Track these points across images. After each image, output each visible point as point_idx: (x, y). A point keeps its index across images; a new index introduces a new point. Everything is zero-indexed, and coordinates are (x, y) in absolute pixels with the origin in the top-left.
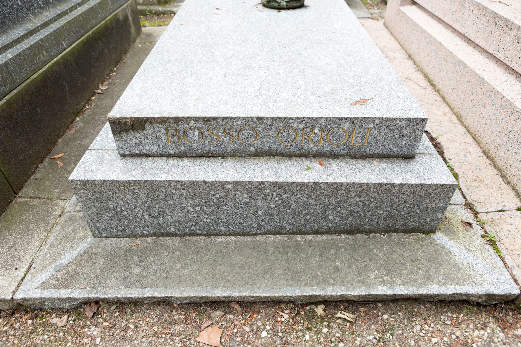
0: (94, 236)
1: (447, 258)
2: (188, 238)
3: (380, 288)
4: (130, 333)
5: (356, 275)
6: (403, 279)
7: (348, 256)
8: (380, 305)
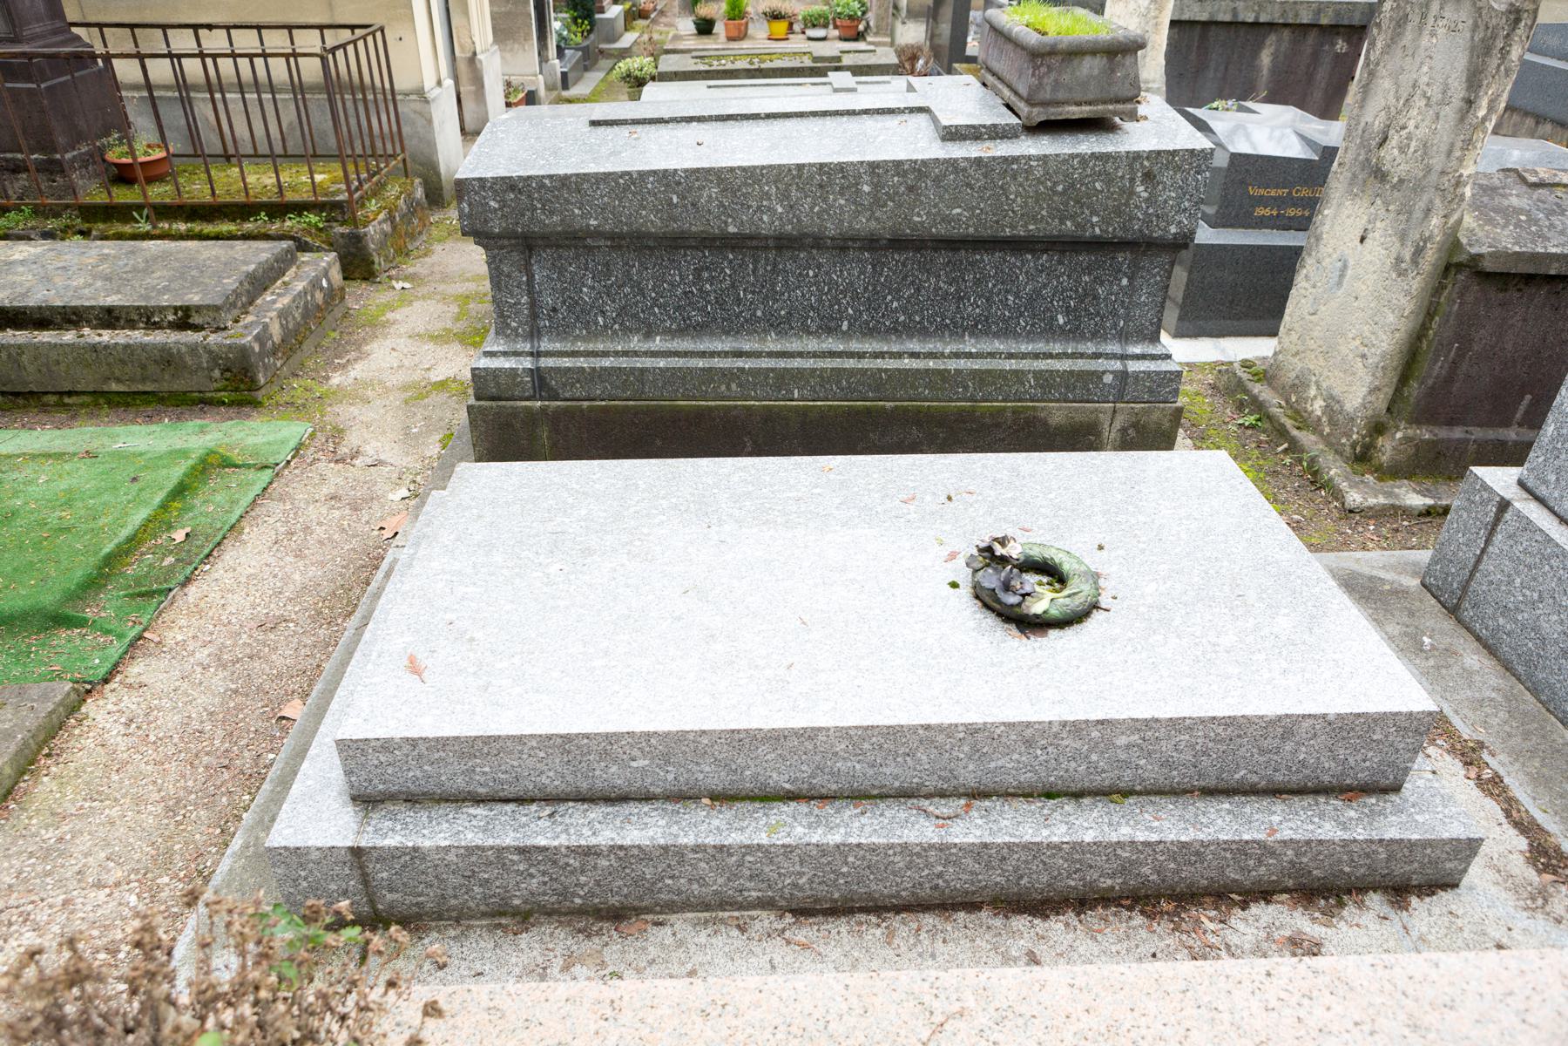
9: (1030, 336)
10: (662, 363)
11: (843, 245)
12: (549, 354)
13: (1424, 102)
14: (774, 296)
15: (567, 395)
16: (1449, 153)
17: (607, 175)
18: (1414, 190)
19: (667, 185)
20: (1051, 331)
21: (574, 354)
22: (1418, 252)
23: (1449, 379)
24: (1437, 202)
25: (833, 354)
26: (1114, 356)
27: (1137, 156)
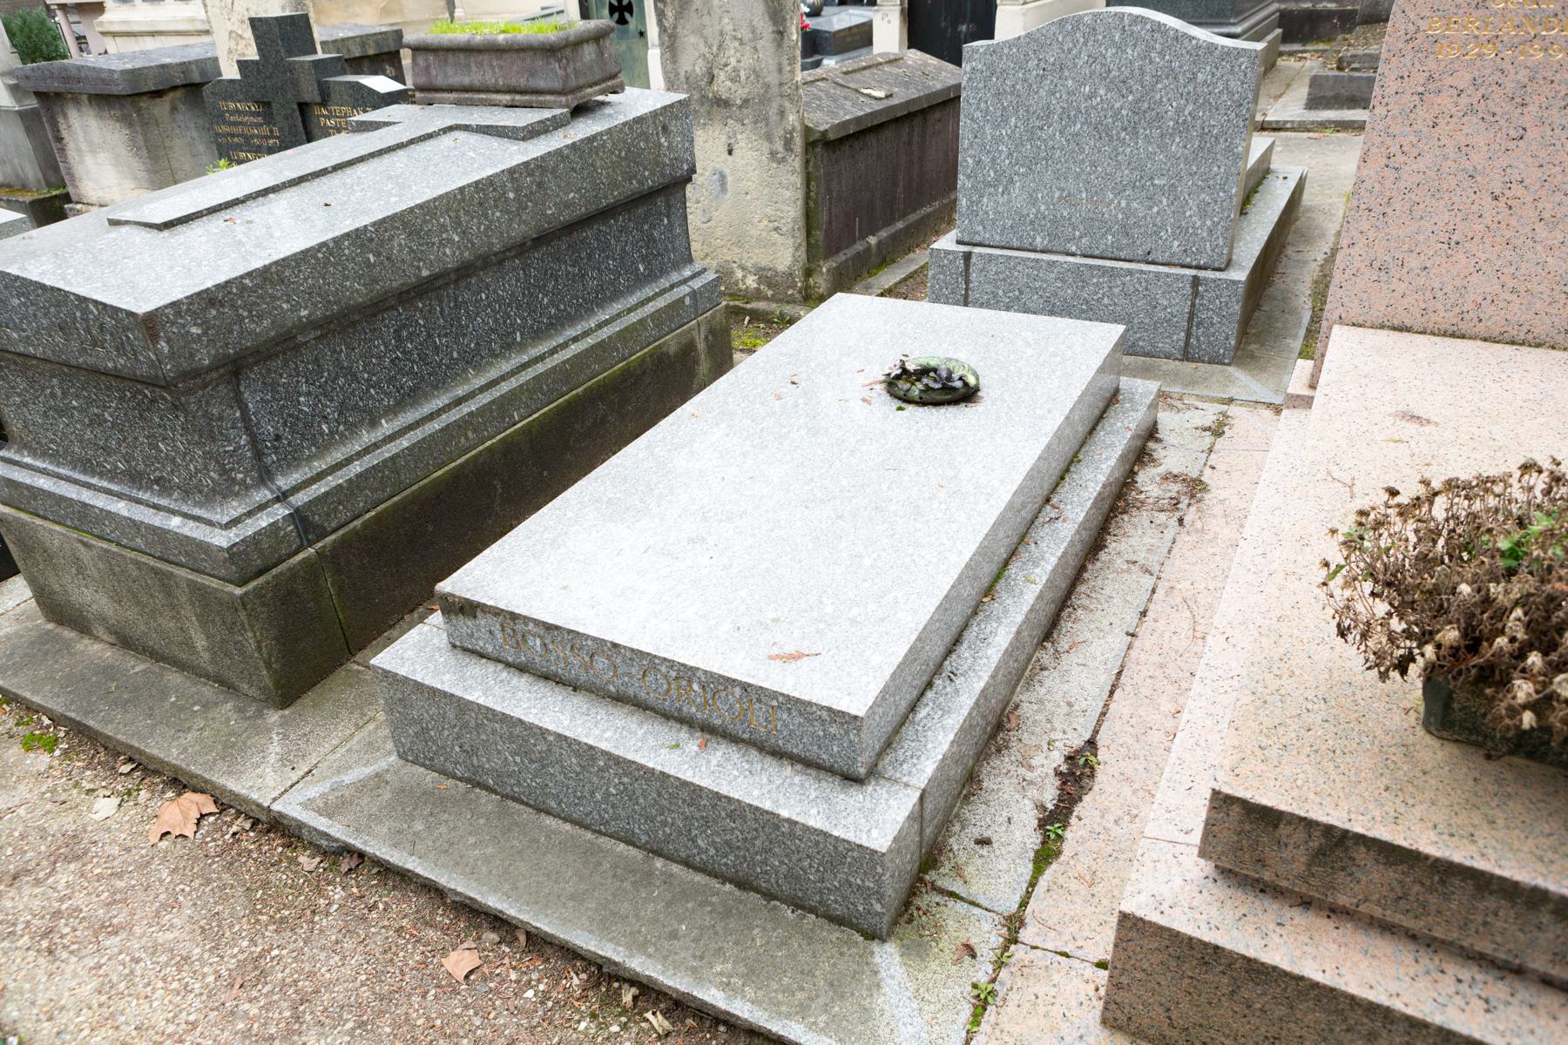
0: (400, 756)
1: (865, 993)
2: (510, 803)
3: (713, 991)
4: (374, 915)
5: (694, 957)
6: (760, 993)
7: (708, 921)
8: (722, 1028)
9: (630, 290)
10: (405, 443)
12: (296, 489)
13: (736, 44)
15: (334, 525)
16: (780, 70)
17: (305, 252)
18: (761, 103)
19: (362, 245)
21: (320, 476)
22: (788, 144)
24: (787, 104)
25: (525, 366)
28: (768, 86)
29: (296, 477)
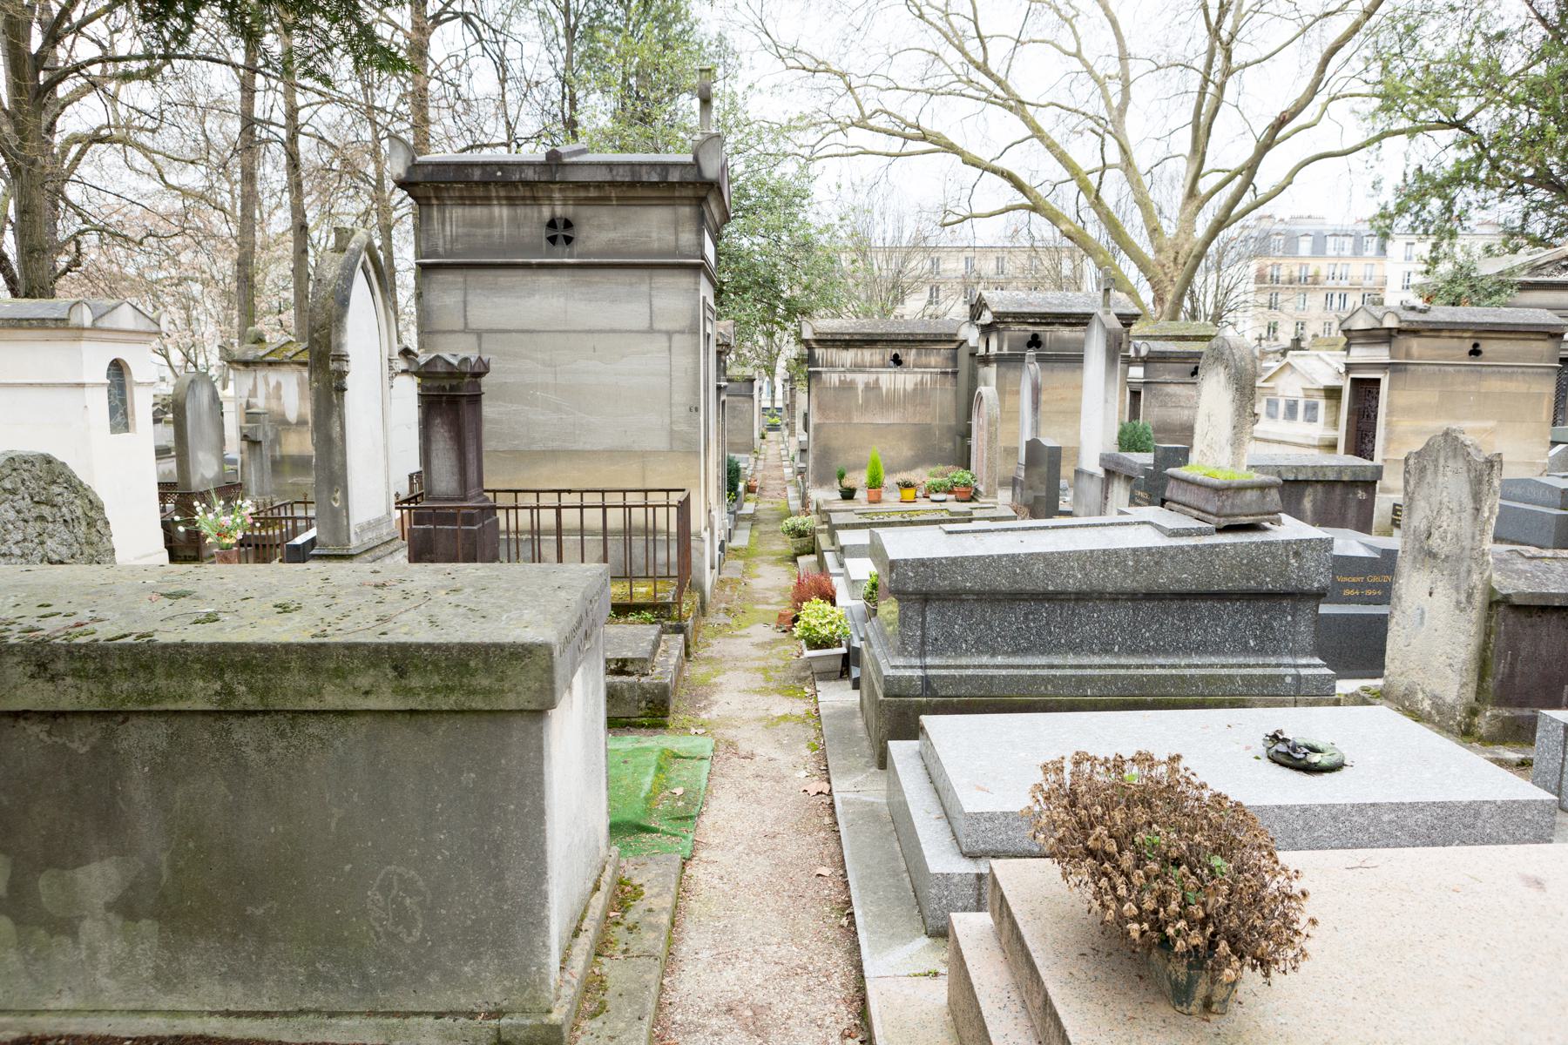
9: (1233, 654)
10: (1004, 672)
11: (1116, 597)
14: (1072, 630)
20: (1246, 650)
21: (948, 667)
22: (1470, 596)
23: (1511, 675)
25: (1111, 666)
26: (1290, 666)
27: (1289, 543)
28: (1463, 549)
29: (937, 661)
